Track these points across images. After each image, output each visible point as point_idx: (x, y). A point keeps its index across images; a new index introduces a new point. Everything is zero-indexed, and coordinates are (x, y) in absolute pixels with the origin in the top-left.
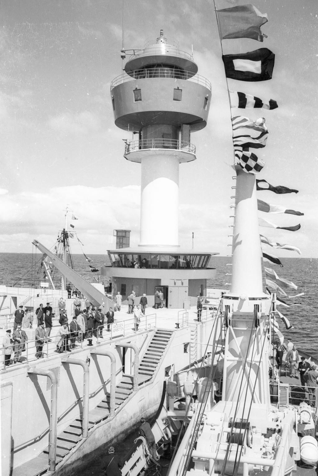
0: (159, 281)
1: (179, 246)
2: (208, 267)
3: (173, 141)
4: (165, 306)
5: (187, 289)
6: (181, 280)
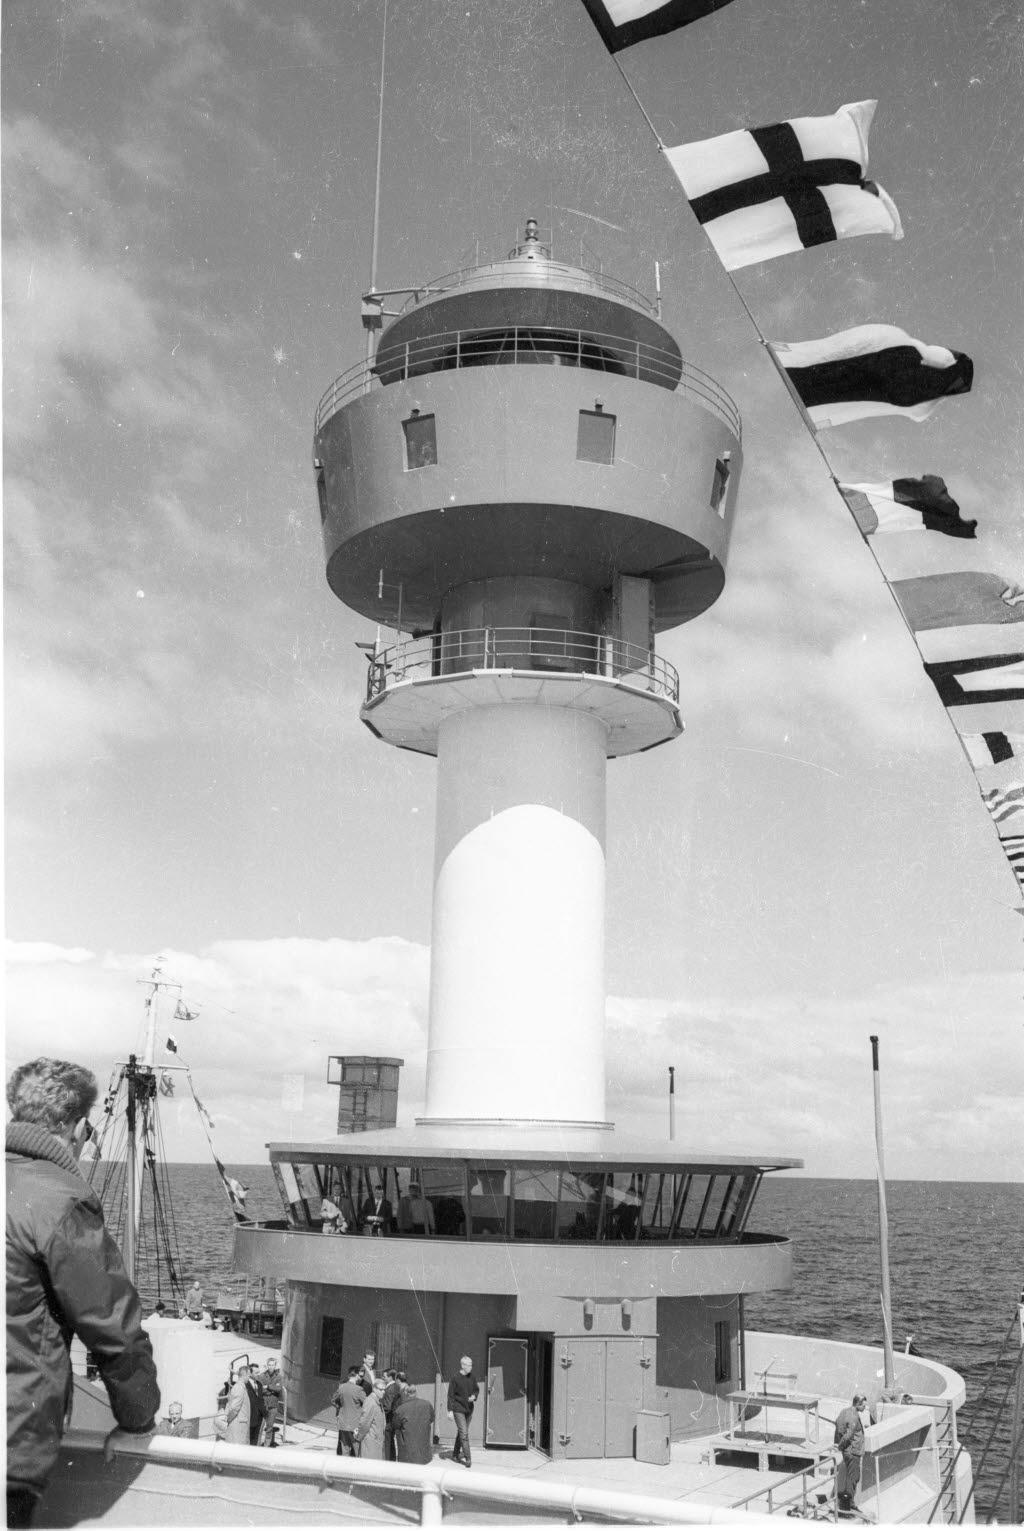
0: (505, 1304)
1: (608, 1126)
2: (749, 1229)
3: (577, 639)
4: (537, 1439)
5: (650, 1351)
6: (618, 1300)
